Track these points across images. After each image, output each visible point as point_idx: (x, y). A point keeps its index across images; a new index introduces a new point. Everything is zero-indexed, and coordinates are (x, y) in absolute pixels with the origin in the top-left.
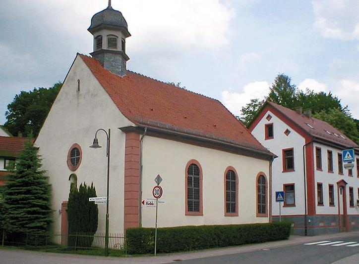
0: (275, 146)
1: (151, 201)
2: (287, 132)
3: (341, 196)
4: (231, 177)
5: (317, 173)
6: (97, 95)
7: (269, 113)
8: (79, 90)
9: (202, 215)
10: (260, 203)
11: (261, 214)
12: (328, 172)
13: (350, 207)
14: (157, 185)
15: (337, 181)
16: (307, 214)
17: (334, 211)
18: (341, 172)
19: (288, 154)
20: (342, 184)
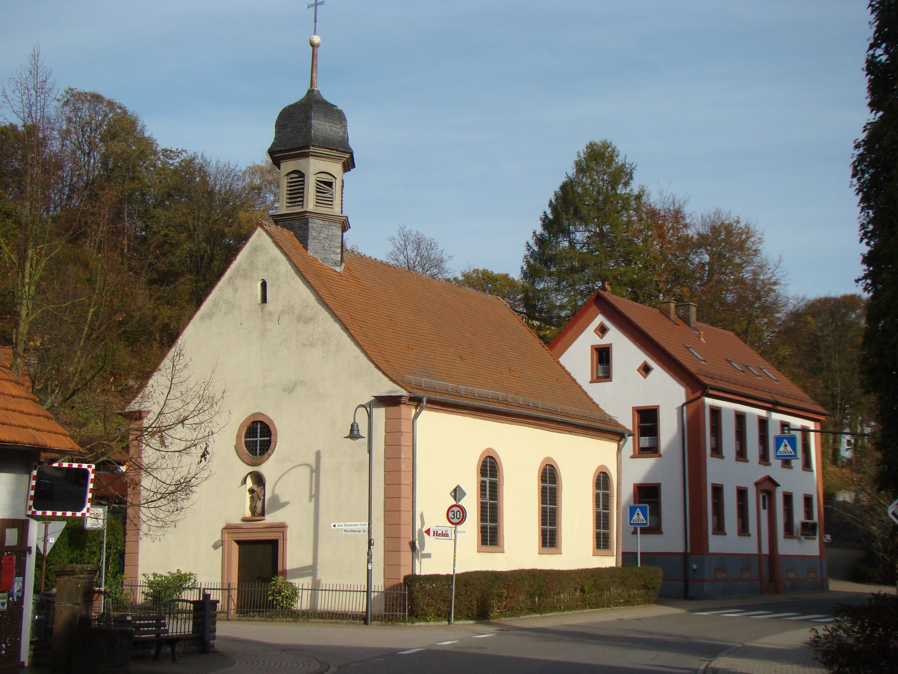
0: (618, 398)
1: (444, 529)
2: (646, 369)
3: (764, 513)
4: (549, 477)
5: (711, 463)
6: (311, 319)
7: (600, 319)
8: (264, 300)
9: (503, 552)
10: (604, 534)
11: (602, 551)
12: (737, 460)
13: (785, 537)
14: (454, 503)
15: (756, 480)
16: (689, 551)
17: (748, 546)
18: (764, 458)
19: (648, 419)
20: (767, 487)
